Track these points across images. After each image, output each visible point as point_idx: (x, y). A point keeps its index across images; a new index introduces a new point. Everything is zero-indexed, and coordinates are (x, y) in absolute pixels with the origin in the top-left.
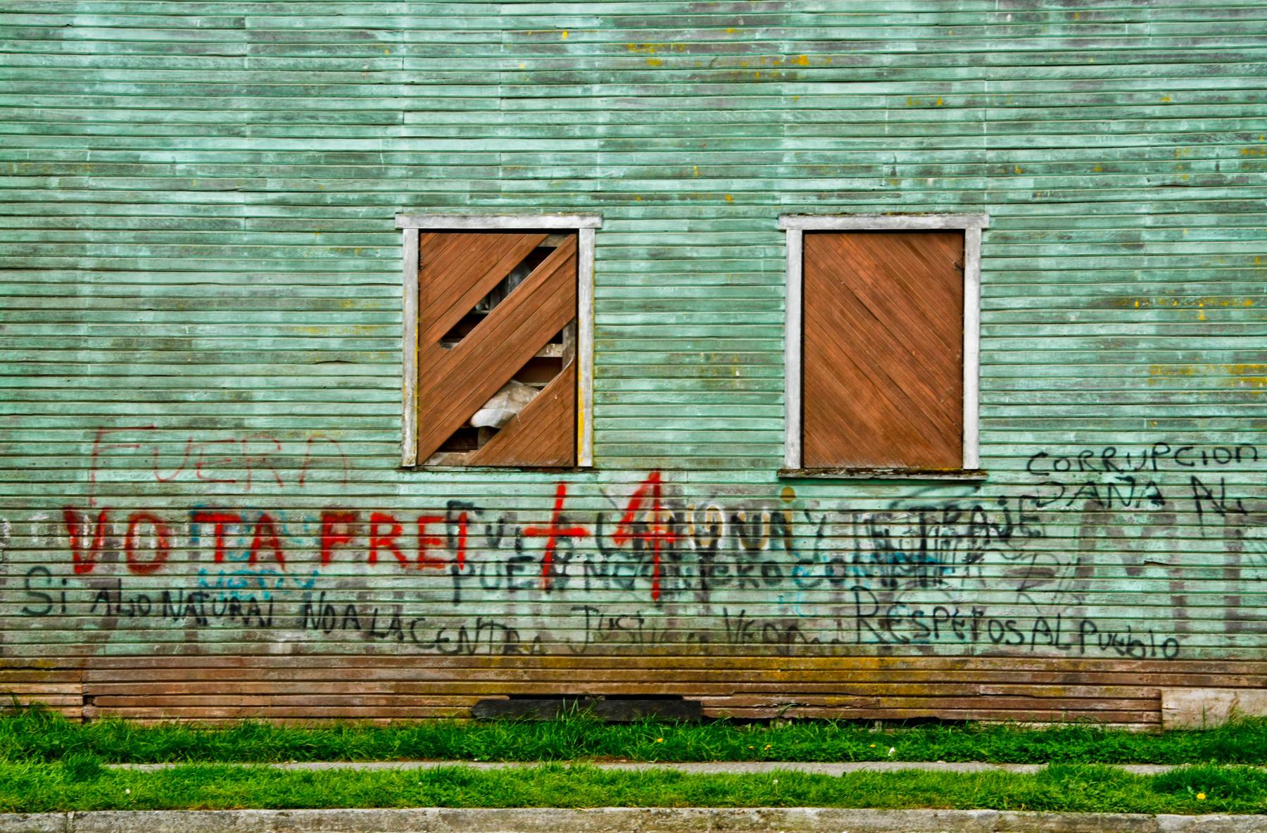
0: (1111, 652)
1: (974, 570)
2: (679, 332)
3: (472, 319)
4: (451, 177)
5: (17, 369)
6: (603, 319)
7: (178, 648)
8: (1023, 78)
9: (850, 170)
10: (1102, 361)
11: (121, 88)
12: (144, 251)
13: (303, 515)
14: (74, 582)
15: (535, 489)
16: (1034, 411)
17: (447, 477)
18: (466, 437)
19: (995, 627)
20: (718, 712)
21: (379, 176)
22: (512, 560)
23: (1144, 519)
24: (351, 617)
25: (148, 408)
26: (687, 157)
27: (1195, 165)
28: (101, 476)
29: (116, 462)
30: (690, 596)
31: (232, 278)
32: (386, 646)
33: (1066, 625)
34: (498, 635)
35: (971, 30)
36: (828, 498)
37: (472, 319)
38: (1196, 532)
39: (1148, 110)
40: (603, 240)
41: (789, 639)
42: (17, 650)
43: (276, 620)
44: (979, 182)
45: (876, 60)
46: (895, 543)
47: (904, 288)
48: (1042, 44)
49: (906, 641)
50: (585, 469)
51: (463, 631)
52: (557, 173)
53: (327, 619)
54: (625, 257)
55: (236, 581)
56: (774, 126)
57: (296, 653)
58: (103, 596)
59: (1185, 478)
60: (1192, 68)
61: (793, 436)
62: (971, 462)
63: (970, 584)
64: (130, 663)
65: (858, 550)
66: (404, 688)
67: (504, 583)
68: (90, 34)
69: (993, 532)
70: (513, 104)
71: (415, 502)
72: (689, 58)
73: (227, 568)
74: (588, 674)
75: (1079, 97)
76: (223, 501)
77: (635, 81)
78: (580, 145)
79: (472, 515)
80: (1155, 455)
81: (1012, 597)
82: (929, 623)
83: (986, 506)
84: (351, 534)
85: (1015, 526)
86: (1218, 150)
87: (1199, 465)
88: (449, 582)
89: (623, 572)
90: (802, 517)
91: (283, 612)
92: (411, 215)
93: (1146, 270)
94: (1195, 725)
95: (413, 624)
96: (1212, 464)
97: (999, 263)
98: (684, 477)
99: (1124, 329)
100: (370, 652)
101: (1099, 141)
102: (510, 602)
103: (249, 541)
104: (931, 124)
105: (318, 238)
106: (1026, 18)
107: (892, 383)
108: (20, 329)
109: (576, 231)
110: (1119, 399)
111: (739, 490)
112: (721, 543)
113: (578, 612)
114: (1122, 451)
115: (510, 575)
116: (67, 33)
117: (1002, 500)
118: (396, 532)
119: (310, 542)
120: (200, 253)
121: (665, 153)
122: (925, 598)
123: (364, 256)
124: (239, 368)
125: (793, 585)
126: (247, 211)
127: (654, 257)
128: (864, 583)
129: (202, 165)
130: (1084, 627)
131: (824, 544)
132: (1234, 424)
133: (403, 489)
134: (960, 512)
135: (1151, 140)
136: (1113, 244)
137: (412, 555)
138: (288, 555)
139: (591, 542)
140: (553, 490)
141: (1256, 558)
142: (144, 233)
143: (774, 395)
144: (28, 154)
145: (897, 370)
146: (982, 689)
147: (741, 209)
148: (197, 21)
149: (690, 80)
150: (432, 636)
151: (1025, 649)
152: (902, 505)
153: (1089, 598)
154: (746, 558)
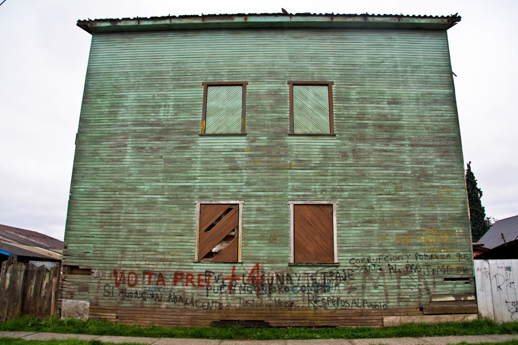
0: (371, 308)
1: (337, 288)
2: (263, 229)
3: (212, 225)
4: (209, 192)
5: (106, 236)
6: (245, 226)
7: (139, 306)
8: (345, 170)
9: (305, 190)
10: (366, 236)
11: (134, 172)
12: (136, 209)
13: (170, 273)
14: (115, 288)
15: (227, 268)
16: (351, 248)
17: (206, 265)
18: (210, 255)
19: (343, 302)
20: (273, 325)
21: (192, 191)
22: (221, 286)
23: (378, 274)
24: (181, 299)
25: (134, 246)
26: (265, 187)
27: (384, 190)
28: (123, 262)
29: (127, 259)
30: (266, 295)
31: (156, 215)
32: (189, 307)
33: (360, 301)
34: (218, 305)
35: (332, 159)
36: (301, 270)
37: (212, 225)
38: (390, 277)
39: (373, 177)
40: (245, 206)
41: (291, 306)
42: (101, 304)
43: (163, 299)
44: (336, 193)
45: (310, 165)
46: (318, 281)
47: (319, 218)
48: (348, 162)
49: (320, 306)
50: (240, 263)
51: (209, 304)
52: (234, 190)
53: (175, 299)
54: (250, 211)
55: (153, 289)
56: (286, 180)
57: (167, 308)
58: (122, 292)
59: (387, 264)
60: (382, 168)
61: (292, 255)
62: (336, 261)
63: (336, 292)
64: (127, 309)
65: (308, 283)
66: (194, 318)
67: (219, 292)
68: (128, 160)
69: (342, 278)
70: (224, 175)
71: (197, 271)
72: (266, 164)
73: (151, 286)
74: (240, 315)
75: (357, 174)
76: (151, 269)
77: (253, 169)
78: (240, 184)
79: (212, 274)
80: (380, 259)
81: (347, 295)
82: (326, 301)
83: (340, 272)
84: (181, 278)
85: (347, 277)
86: (389, 187)
87: (390, 261)
88: (205, 291)
89: (249, 289)
90: (294, 275)
91: (164, 297)
92: (199, 200)
93: (375, 214)
94: (391, 325)
95: (196, 301)
96: (393, 261)
97: (341, 212)
98: (265, 265)
99: (371, 228)
100: (185, 308)
101: (363, 184)
102: (221, 296)
103: (157, 279)
104: (323, 180)
105: (176, 206)
106: (344, 156)
107: (316, 241)
108: (107, 227)
109: (238, 204)
110: (371, 245)
111: (278, 268)
112: (274, 282)
113: (237, 299)
114: (372, 258)
115: (221, 289)
116: (124, 160)
117: (344, 270)
118: (193, 278)
119: (171, 280)
120: (149, 209)
121: (260, 186)
122: (325, 295)
123: (187, 210)
124: (156, 237)
125: (292, 292)
126: (160, 200)
127: (257, 210)
128: (310, 292)
129: (150, 189)
130: (364, 301)
131: (300, 282)
132: (397, 251)
133: (194, 267)
134: (333, 273)
135: (374, 184)
136: (367, 208)
137: (196, 284)
138: (166, 283)
139: (241, 281)
140: (232, 268)
141: (404, 283)
142: (137, 205)
143: (287, 244)
144: (112, 187)
145: (317, 238)
146: (340, 318)
147: (279, 199)
148: (152, 157)
149: (266, 169)
150: (201, 304)
151: (350, 308)
152: (319, 272)
153: (366, 294)
154: (280, 285)
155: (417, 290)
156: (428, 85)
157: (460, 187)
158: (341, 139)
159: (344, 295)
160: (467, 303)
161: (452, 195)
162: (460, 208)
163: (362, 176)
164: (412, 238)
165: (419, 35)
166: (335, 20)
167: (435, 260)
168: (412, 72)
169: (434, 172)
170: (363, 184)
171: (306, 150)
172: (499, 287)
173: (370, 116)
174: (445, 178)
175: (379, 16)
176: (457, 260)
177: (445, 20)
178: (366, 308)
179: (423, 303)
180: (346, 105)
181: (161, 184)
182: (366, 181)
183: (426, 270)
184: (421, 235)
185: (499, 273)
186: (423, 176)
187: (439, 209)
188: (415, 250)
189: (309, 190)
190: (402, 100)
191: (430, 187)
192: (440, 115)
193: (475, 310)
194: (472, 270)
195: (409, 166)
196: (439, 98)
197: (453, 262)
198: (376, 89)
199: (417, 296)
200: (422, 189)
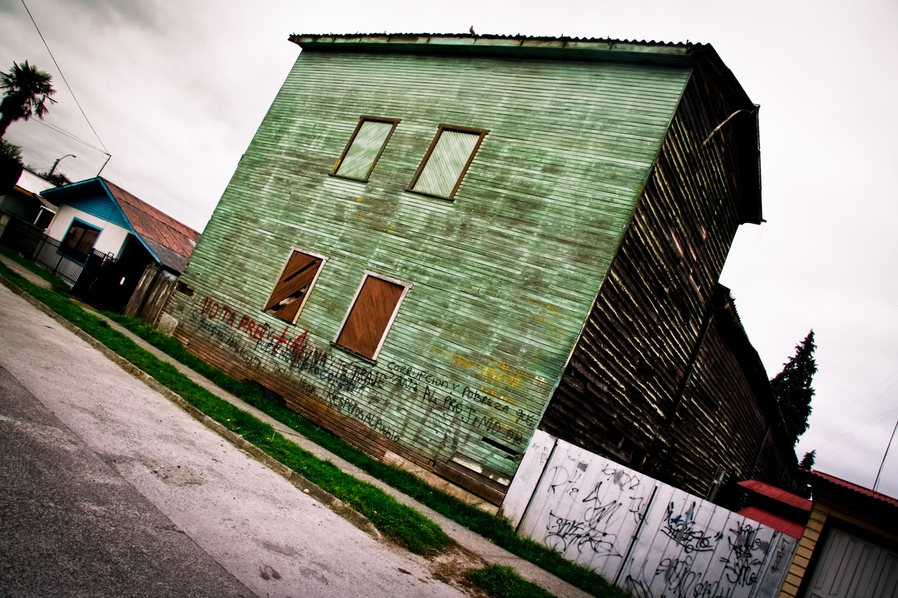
0: (381, 432)
16: (398, 348)
23: (409, 394)
26: (354, 247)
32: (237, 355)
35: (433, 230)
36: (338, 355)
41: (311, 392)
44: (415, 274)
48: (450, 239)
66: (235, 368)
81: (365, 403)
85: (377, 383)
86: (481, 285)
93: (446, 316)
96: (434, 385)
97: (409, 300)
101: (451, 272)
112: (311, 358)
113: (270, 360)
114: (413, 370)
117: (377, 373)
127: (335, 272)
131: (332, 368)
135: (465, 276)
136: (440, 304)
145: (372, 324)
153: (384, 413)
155: (442, 437)
156: (615, 151)
157: (577, 315)
158: (457, 207)
159: (363, 402)
160: (492, 485)
161: (560, 323)
162: (561, 347)
163: (457, 261)
164: (472, 364)
165: (645, 73)
166: (526, 44)
167: (486, 407)
168: (603, 129)
169: (553, 282)
170: (451, 272)
171: (413, 213)
172: (553, 486)
173: (509, 184)
174: (562, 296)
175: (585, 40)
176: (514, 419)
177: (684, 50)
178: (377, 430)
179: (440, 457)
180: (488, 164)
181: (277, 221)
182: (457, 269)
183: (467, 415)
184: (487, 364)
185: (565, 465)
186: (535, 283)
187: (529, 336)
188: (469, 381)
189: (391, 262)
190: (564, 169)
191: (534, 301)
192: (608, 199)
193: (498, 501)
194: (526, 442)
195: (522, 264)
196: (620, 174)
197: (507, 420)
198: (538, 148)
199: (438, 444)
200: (522, 302)
